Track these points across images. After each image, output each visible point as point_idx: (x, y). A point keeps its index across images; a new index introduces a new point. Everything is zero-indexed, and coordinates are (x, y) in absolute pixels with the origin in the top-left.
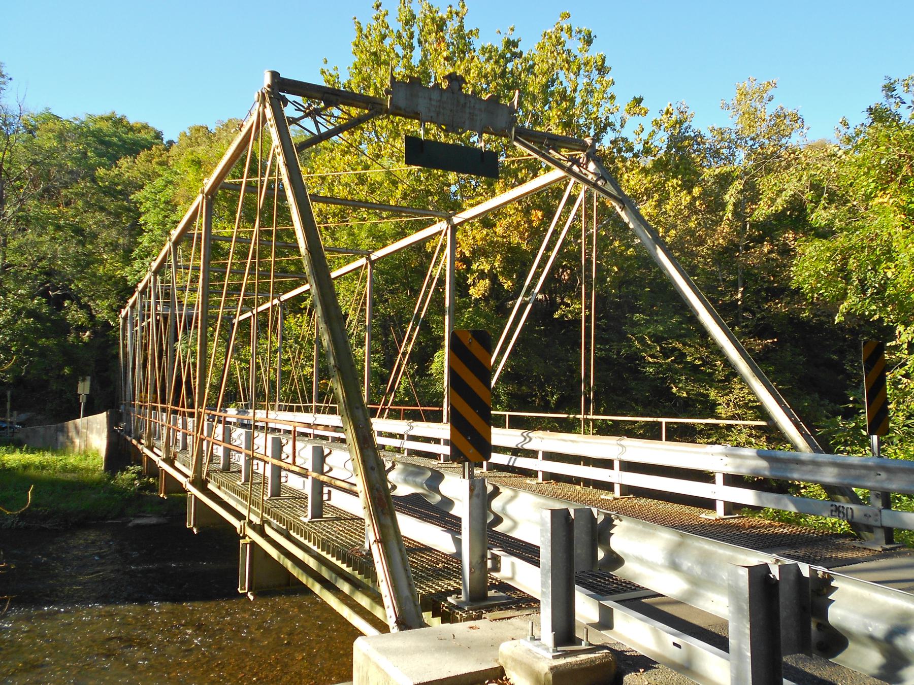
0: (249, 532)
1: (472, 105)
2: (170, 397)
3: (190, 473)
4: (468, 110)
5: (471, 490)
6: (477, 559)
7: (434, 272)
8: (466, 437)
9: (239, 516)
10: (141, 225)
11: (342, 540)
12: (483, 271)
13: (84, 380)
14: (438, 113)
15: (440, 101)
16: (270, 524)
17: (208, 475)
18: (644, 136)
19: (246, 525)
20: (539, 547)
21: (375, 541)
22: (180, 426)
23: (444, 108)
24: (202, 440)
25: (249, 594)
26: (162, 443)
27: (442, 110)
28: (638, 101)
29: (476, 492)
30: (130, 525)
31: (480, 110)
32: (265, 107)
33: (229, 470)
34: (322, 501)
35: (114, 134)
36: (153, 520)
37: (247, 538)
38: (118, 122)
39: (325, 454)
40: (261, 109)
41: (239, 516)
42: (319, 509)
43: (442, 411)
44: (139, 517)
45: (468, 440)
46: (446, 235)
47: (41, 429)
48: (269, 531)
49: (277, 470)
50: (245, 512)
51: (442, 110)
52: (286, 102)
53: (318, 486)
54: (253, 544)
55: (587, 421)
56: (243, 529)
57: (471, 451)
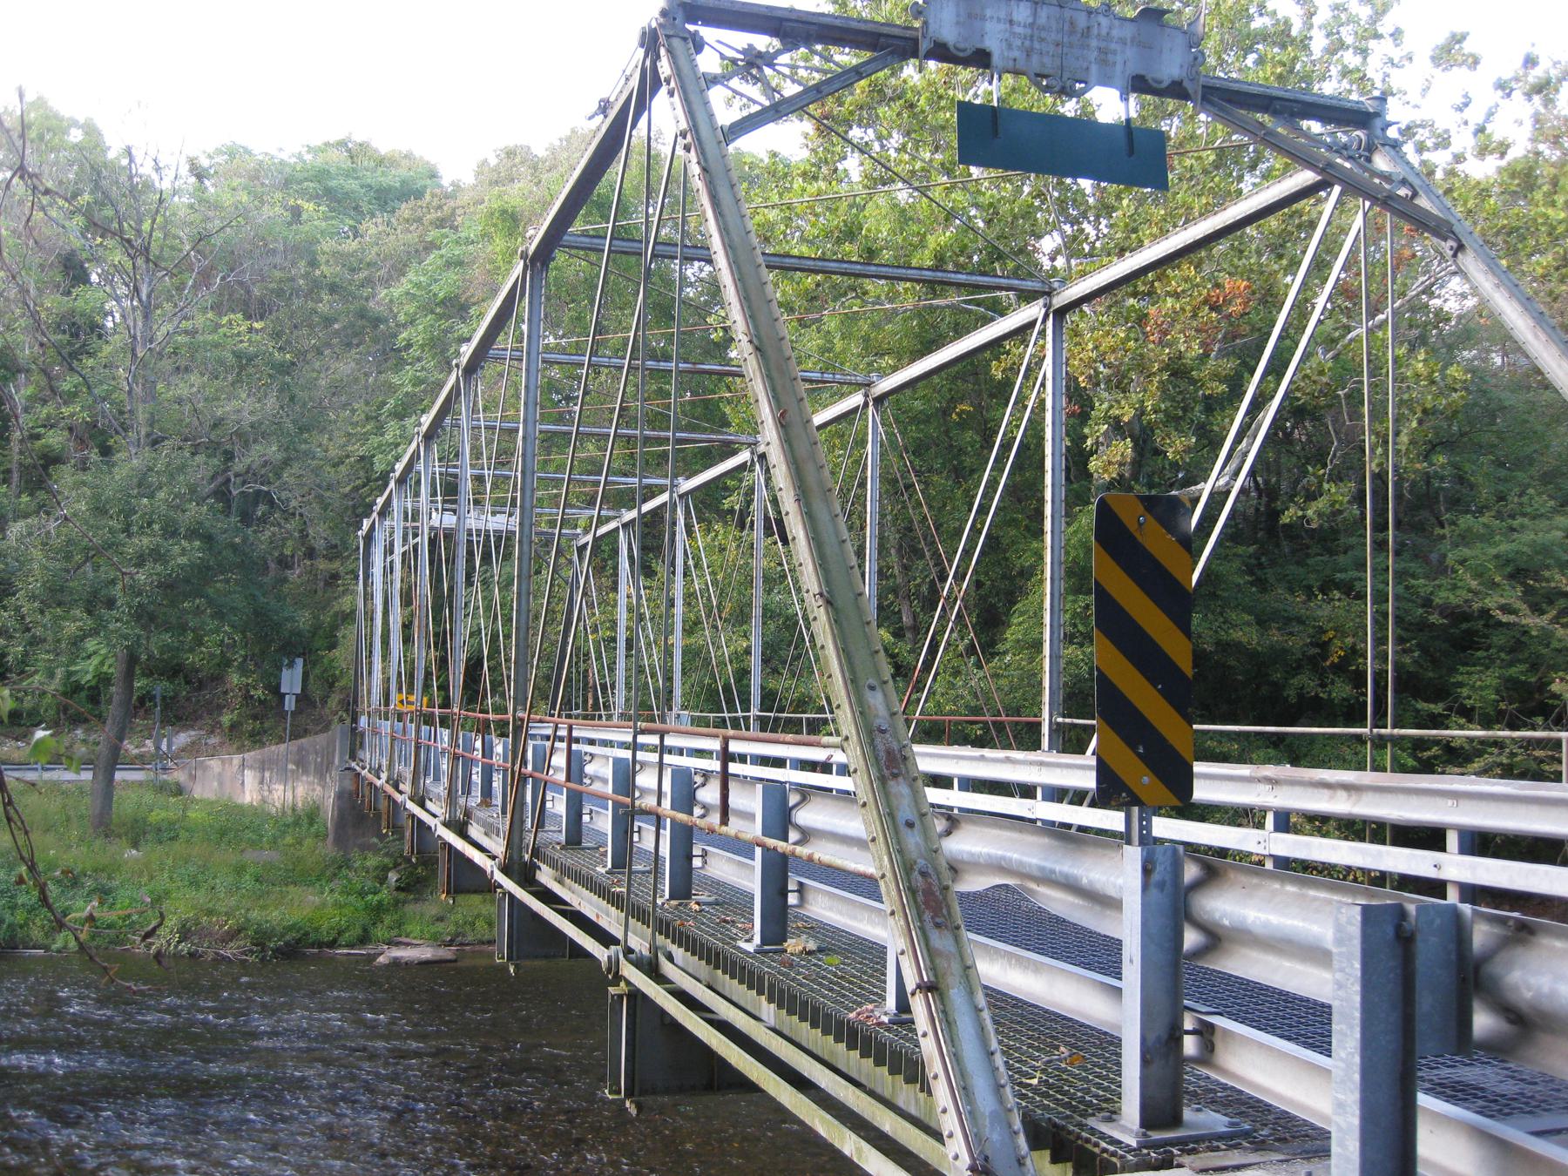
0: (629, 972)
1: (1104, 32)
2: (456, 693)
3: (498, 846)
4: (1094, 43)
5: (1147, 871)
6: (1160, 1030)
7: (1010, 424)
8: (1134, 748)
9: (606, 939)
10: (399, 350)
11: (831, 990)
12: (1117, 419)
13: (291, 665)
14: (1029, 53)
15: (1032, 25)
16: (670, 958)
17: (536, 852)
18: (1475, 115)
19: (621, 956)
20: (1330, 1007)
21: (919, 986)
22: (478, 754)
23: (1042, 40)
24: (523, 779)
25: (628, 1104)
26: (441, 789)
27: (1037, 45)
28: (1458, 39)
29: (1156, 877)
30: (381, 959)
31: (1123, 41)
32: (658, 57)
33: (579, 843)
34: (785, 905)
35: (348, 174)
36: (425, 953)
37: (622, 984)
38: (356, 152)
39: (790, 805)
40: (648, 63)
41: (606, 939)
42: (778, 922)
43: (1039, 724)
44: (398, 944)
45: (1139, 755)
46: (1042, 333)
47: (214, 764)
48: (668, 968)
49: (684, 838)
50: (617, 932)
51: (1037, 45)
52: (699, 45)
53: (778, 870)
54: (636, 996)
55: (1380, 743)
56: (614, 965)
57: (1144, 780)
